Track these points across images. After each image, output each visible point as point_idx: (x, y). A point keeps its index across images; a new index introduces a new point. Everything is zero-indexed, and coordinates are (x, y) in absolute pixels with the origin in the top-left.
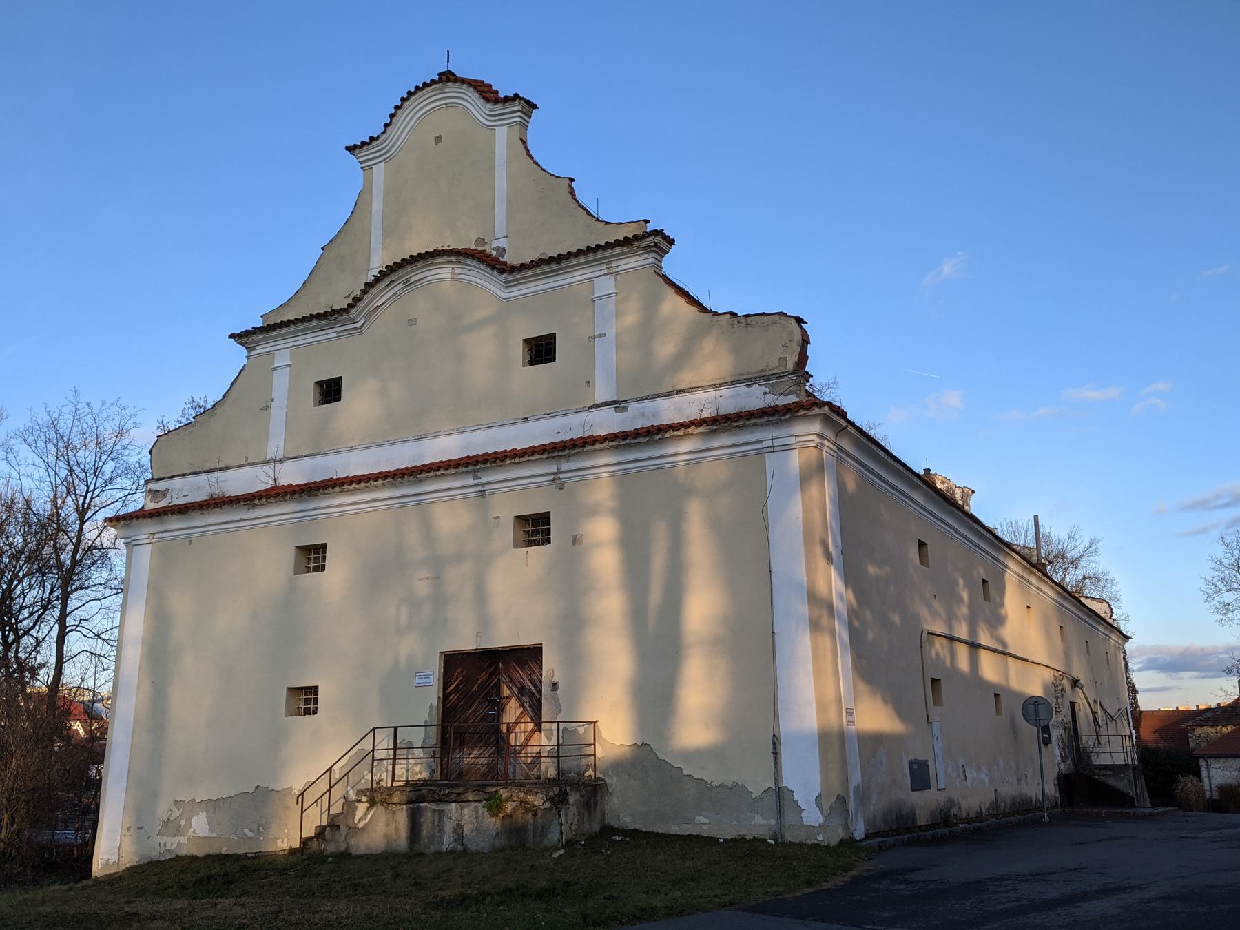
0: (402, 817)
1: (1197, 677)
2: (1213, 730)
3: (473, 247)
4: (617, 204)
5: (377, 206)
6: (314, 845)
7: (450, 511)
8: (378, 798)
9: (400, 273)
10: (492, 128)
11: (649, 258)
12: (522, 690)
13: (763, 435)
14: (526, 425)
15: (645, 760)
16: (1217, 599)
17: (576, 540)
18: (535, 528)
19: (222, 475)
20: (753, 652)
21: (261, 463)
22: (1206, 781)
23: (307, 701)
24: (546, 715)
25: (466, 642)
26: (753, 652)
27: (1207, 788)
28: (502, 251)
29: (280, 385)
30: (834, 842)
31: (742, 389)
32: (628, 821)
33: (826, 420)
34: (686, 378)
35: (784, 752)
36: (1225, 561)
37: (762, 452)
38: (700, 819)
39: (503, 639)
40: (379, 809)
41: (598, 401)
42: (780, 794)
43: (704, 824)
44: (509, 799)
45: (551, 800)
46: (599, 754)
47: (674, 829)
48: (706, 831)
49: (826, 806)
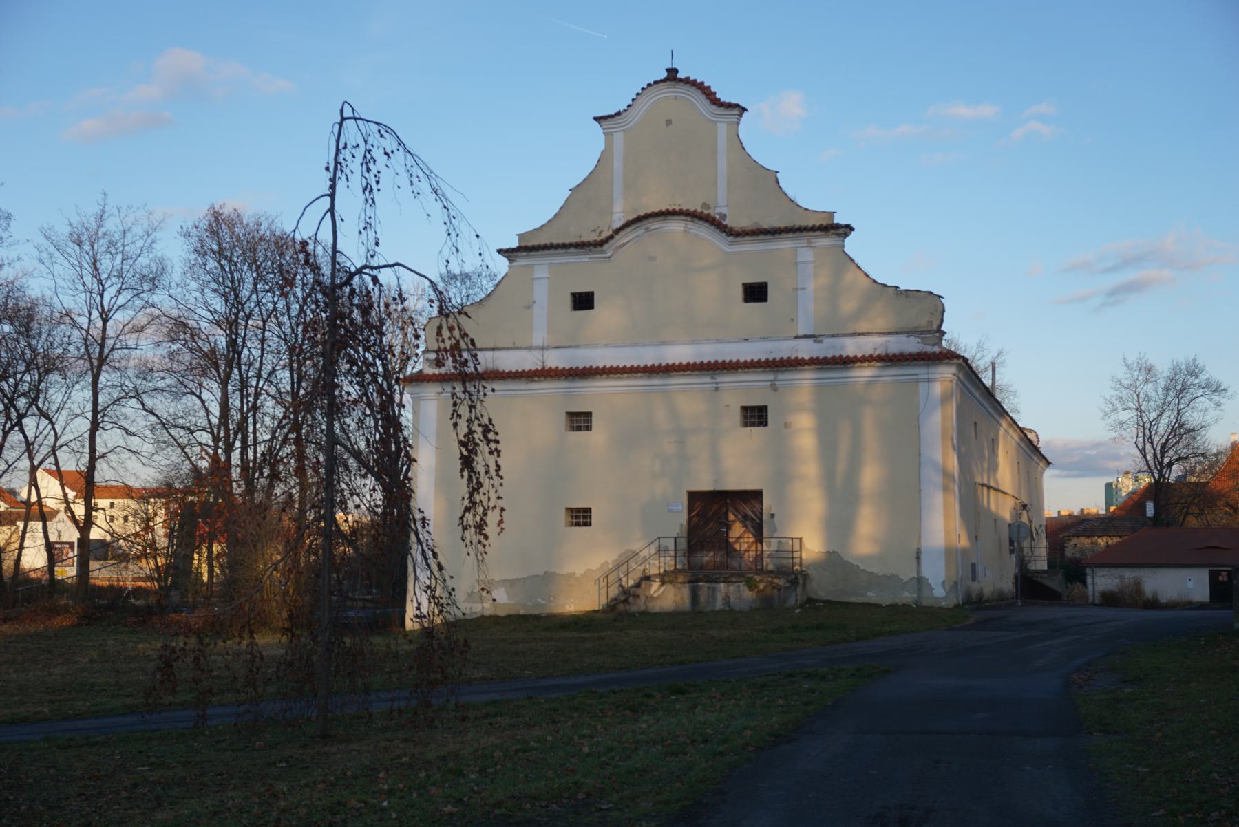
0: (686, 591)
1: (1058, 476)
2: (1089, 541)
3: (699, 210)
4: (810, 193)
5: (618, 165)
6: (621, 607)
7: (689, 397)
8: (666, 579)
9: (645, 222)
10: (715, 123)
11: (837, 241)
12: (745, 517)
13: (920, 371)
14: (746, 344)
15: (833, 560)
16: (1113, 417)
17: (787, 425)
18: (755, 416)
19: (497, 353)
20: (904, 501)
21: (530, 348)
22: (1090, 587)
23: (585, 517)
24: (766, 533)
25: (705, 484)
26: (904, 501)
27: (1090, 594)
28: (724, 217)
29: (541, 292)
30: (951, 605)
31: (903, 338)
32: (823, 595)
33: (959, 367)
34: (863, 326)
35: (923, 557)
36: (1125, 382)
37: (917, 381)
38: (870, 594)
39: (732, 484)
40: (669, 587)
41: (801, 333)
42: (920, 581)
43: (872, 596)
44: (761, 581)
45: (791, 582)
46: (804, 556)
47: (853, 599)
48: (873, 601)
49: (947, 587)
